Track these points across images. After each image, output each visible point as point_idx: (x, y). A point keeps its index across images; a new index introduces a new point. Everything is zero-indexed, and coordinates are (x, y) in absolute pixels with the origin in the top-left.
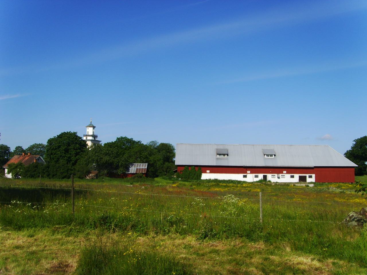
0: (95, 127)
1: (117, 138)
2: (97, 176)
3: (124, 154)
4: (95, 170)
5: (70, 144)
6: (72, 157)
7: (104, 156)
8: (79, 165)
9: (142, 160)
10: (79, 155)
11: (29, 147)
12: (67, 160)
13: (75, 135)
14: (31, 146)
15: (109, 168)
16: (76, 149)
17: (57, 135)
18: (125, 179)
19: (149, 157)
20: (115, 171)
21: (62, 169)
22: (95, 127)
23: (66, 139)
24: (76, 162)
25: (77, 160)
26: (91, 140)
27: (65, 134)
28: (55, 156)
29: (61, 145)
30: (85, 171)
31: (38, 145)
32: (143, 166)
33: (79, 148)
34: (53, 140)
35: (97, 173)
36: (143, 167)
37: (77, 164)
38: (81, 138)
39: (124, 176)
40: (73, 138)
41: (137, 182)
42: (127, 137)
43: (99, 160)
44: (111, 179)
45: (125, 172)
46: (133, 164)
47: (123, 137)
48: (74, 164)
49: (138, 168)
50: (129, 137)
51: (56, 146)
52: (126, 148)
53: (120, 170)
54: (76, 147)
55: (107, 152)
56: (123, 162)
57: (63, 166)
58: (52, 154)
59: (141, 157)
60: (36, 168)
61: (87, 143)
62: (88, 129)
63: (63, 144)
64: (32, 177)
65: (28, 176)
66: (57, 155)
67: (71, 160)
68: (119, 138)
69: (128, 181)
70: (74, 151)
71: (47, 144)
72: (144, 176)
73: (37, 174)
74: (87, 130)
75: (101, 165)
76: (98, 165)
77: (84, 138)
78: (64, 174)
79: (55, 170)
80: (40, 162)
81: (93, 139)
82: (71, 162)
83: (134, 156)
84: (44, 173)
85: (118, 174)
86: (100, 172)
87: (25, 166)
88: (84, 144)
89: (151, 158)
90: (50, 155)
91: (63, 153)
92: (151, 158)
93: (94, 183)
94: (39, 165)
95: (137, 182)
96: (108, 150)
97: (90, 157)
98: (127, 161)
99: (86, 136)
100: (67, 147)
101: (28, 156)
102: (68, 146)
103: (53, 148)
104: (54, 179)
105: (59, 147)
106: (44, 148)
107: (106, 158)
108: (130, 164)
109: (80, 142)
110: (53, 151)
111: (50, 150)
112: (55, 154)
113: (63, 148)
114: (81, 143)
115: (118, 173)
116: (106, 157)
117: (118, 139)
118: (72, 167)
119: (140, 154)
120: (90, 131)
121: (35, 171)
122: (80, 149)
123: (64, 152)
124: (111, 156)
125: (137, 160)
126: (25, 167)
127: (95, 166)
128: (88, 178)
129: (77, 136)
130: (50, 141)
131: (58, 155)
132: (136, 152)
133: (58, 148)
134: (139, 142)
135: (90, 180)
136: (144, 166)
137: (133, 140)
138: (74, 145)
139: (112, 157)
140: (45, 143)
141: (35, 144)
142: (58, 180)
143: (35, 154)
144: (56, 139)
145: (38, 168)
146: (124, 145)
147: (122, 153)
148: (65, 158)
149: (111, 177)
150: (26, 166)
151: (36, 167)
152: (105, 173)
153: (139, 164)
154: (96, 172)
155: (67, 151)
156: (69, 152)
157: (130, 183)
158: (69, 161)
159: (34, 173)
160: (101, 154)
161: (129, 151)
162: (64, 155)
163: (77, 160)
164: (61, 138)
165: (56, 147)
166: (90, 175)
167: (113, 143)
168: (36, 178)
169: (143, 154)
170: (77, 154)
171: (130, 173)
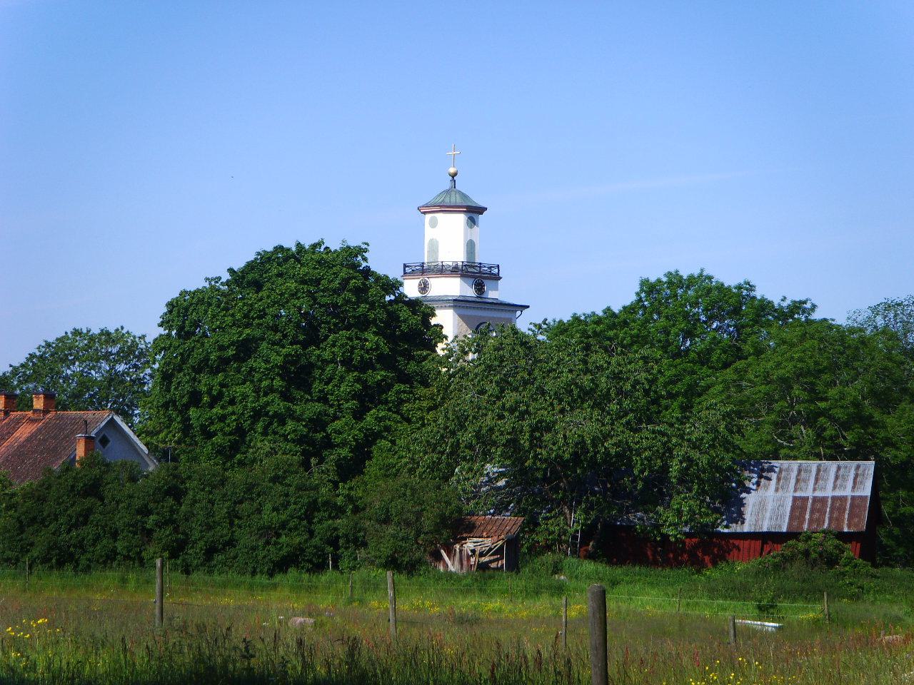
0: (481, 210)
1: (74, 329)
2: (514, 554)
3: (694, 392)
4: (500, 508)
5: (323, 331)
6: (335, 418)
7: (562, 411)
8: (389, 472)
9: (827, 433)
10: (386, 402)
11: (32, 356)
12: (299, 441)
13: (355, 266)
14: (48, 345)
15: (594, 493)
16: (365, 366)
17: (231, 271)
18: (713, 574)
19: (877, 416)
20: (637, 518)
21: (268, 506)
22: (481, 210)
23: (294, 295)
24: (362, 451)
25: (371, 438)
26: (458, 304)
27: (286, 260)
28: (217, 410)
29: (258, 333)
30: (427, 523)
31: (92, 339)
32: (845, 479)
33: (381, 358)
34: (201, 301)
35: (515, 529)
36: (843, 487)
37: (372, 468)
38: (391, 286)
39: (707, 549)
40: (336, 284)
41: (810, 593)
42: (710, 278)
43: (524, 441)
44: (619, 571)
45: (714, 525)
46: (771, 469)
47: (685, 274)
48: (350, 469)
49: (808, 492)
50: (729, 277)
51: (225, 340)
52: (709, 351)
53: (679, 513)
54: (362, 348)
55: (586, 380)
56: (695, 455)
57: (275, 479)
58: (195, 398)
59: (822, 413)
60: (89, 502)
61: (433, 321)
62: (434, 224)
63: (275, 329)
64: (60, 564)
65: (35, 552)
66: (230, 409)
67: (328, 444)
68: (653, 279)
69: (738, 591)
70: (351, 377)
71: (162, 331)
72: (850, 551)
73: (97, 539)
74: (429, 233)
75: (539, 475)
76: (521, 476)
77: (411, 289)
78: (283, 539)
79: (222, 510)
80: (115, 454)
81: (470, 292)
82: (332, 456)
83: (770, 410)
84: (149, 533)
85: (665, 537)
86: (532, 524)
87: (16, 488)
88: (408, 328)
89: (889, 420)
90: (187, 407)
91: (271, 389)
92: (889, 420)
93: (496, 604)
94: (109, 477)
95: (807, 600)
96: (587, 371)
97: (462, 422)
98: (728, 446)
99: (423, 270)
100: (300, 351)
101: (30, 413)
102: (305, 345)
103: (207, 359)
104: (217, 577)
105: (246, 349)
106: (139, 357)
107: (581, 425)
108: (745, 467)
109: (390, 314)
110: (206, 382)
111: (180, 370)
112: (215, 400)
113: (273, 357)
114: (393, 318)
115: (664, 530)
116: (578, 416)
117: (649, 288)
118: (336, 486)
119: (815, 396)
120: (448, 238)
121: (84, 518)
122: (386, 361)
123: (278, 383)
124: (614, 407)
125: (791, 438)
126: (13, 495)
127: (502, 483)
128: (453, 566)
129: (367, 272)
130: (184, 313)
131: (238, 408)
132: (786, 383)
133: (236, 358)
134: (797, 307)
135: (469, 581)
136: (849, 482)
137: (758, 294)
138: (350, 339)
139: (621, 418)
140: (147, 325)
141: (77, 332)
142: (248, 578)
143: (76, 399)
144: (224, 294)
145: (102, 499)
146: (689, 334)
147: (680, 387)
148: (290, 425)
149: (610, 562)
150: (17, 487)
151: (94, 489)
152: (571, 531)
153: (813, 465)
154: (511, 522)
155: (298, 376)
156: (317, 386)
157: (752, 604)
158: (314, 445)
159: (74, 533)
160: (543, 393)
161: (729, 374)
162: (278, 405)
163: (371, 438)
164: (258, 286)
165: (222, 348)
166: (469, 545)
167: (611, 320)
168: (87, 569)
169: (832, 392)
170: (367, 398)
171: (746, 528)
